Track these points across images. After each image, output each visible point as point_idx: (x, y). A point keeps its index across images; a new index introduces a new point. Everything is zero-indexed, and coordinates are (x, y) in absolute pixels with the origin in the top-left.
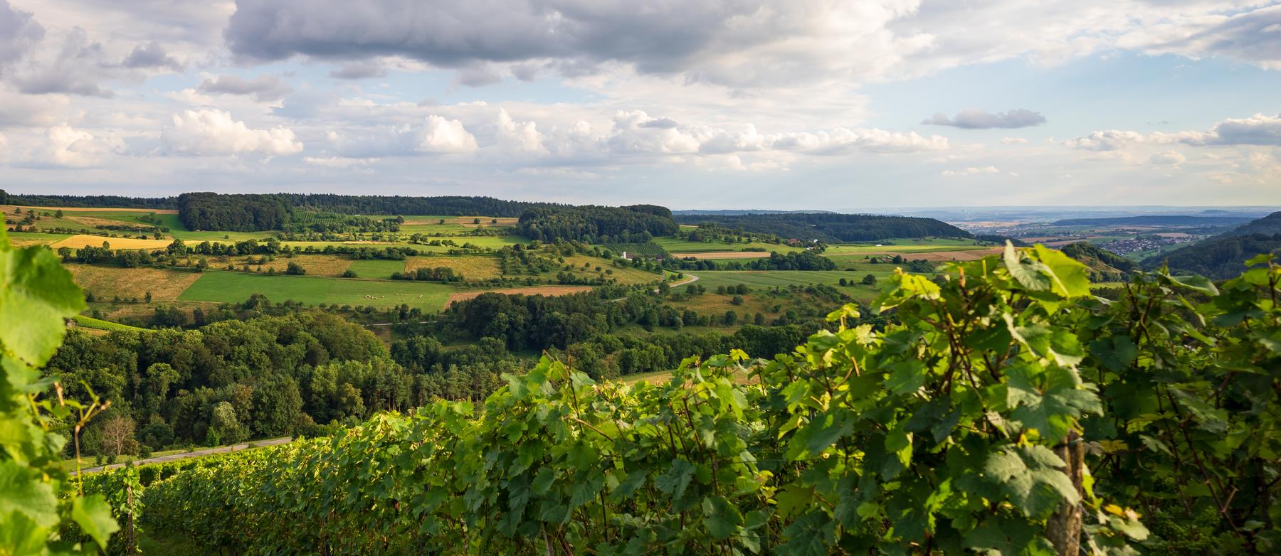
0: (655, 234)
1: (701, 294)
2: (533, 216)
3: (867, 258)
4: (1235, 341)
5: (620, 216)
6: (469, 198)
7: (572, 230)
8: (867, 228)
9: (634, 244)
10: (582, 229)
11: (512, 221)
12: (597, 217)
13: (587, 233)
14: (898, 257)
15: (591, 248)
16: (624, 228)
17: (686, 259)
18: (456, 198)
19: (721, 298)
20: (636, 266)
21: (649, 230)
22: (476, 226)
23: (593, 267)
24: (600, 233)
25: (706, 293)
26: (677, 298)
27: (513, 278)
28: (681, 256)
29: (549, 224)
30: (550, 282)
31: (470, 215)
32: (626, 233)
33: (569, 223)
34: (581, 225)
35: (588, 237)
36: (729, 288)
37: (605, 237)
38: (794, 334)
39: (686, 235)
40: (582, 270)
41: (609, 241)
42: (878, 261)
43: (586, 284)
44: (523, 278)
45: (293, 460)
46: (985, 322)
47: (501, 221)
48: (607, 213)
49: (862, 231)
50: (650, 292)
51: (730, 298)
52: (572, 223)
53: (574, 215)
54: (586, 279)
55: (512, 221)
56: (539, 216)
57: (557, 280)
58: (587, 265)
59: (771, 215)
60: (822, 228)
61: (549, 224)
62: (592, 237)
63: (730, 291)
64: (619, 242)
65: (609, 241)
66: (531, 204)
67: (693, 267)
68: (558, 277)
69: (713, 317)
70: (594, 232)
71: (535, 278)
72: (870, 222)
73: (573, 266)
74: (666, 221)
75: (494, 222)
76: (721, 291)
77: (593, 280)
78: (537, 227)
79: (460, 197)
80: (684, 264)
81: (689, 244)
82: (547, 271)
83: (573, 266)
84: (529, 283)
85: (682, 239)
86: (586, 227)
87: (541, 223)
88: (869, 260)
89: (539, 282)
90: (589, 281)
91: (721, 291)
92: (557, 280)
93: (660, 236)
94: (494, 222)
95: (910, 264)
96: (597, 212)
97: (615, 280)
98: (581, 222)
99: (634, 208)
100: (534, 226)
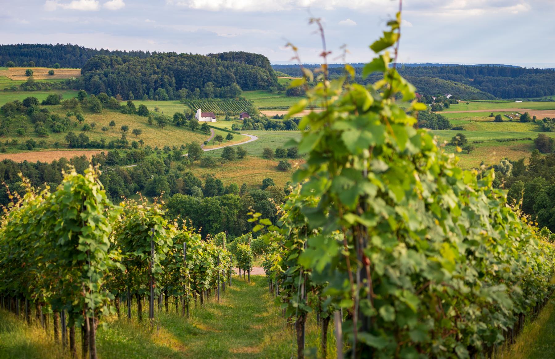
0: (246, 87)
1: (241, 158)
2: (97, 66)
3: (492, 116)
4: (85, 195)
5: (204, 66)
6: (50, 46)
7: (143, 83)
8: (531, 83)
9: (219, 100)
10: (156, 82)
11: (73, 73)
12: (175, 67)
13: (162, 86)
14: (526, 115)
15: (124, 103)
16: (209, 80)
17: (276, 117)
18: (32, 46)
19: (266, 162)
20: (178, 125)
21: (238, 83)
22: (26, 79)
23: (118, 126)
24: (179, 87)
25: (248, 156)
26: (208, 163)
27: (10, 140)
28: (270, 114)
29: (115, 76)
30: (56, 146)
31: (47, 66)
32: (210, 87)
33: (140, 74)
34: (154, 77)
35: (162, 91)
36: (277, 151)
37: (184, 92)
38: (229, 205)
39: (284, 89)
40: (104, 129)
41: (188, 96)
42: (504, 118)
43: (103, 147)
44: (22, 141)
45: (194, 349)
46: (20, 175)
47: (59, 72)
48: (187, 62)
49: (523, 87)
50: (178, 157)
51: (276, 162)
52: (144, 75)
53: (148, 65)
54: (103, 141)
55: (73, 73)
56: (105, 67)
57: (66, 143)
58: (112, 124)
59: (425, 68)
60: (480, 83)
61: (115, 76)
62: (167, 91)
63: (280, 154)
64: (201, 97)
65: (188, 96)
66: (148, 53)
67: (280, 126)
68: (67, 138)
69: (244, 186)
70: (170, 85)
71: (38, 140)
72: (534, 76)
73: (93, 125)
74: (262, 73)
75: (51, 73)
76: (267, 154)
77: (113, 142)
78: (100, 79)
79: (39, 46)
80: (269, 123)
81: (287, 99)
82: (58, 132)
83: (93, 125)
84: (30, 146)
85: (279, 93)
86: (162, 79)
87: (106, 75)
88: (493, 118)
89: (42, 145)
90: (107, 143)
91: (267, 154)
92: (66, 143)
93: (254, 89)
94: (51, 73)
95: (539, 123)
96: (176, 61)
97: (141, 142)
98: (155, 73)
99: (223, 56)
100: (96, 78)
